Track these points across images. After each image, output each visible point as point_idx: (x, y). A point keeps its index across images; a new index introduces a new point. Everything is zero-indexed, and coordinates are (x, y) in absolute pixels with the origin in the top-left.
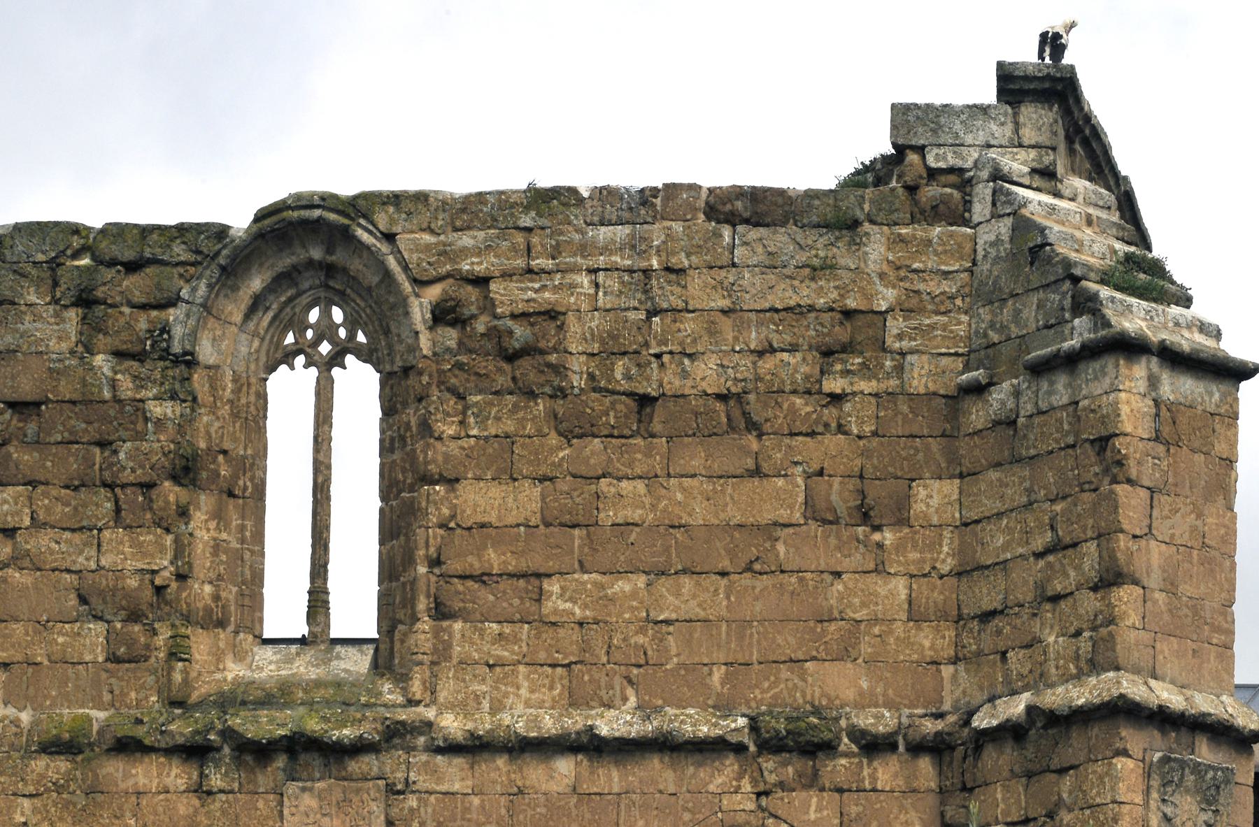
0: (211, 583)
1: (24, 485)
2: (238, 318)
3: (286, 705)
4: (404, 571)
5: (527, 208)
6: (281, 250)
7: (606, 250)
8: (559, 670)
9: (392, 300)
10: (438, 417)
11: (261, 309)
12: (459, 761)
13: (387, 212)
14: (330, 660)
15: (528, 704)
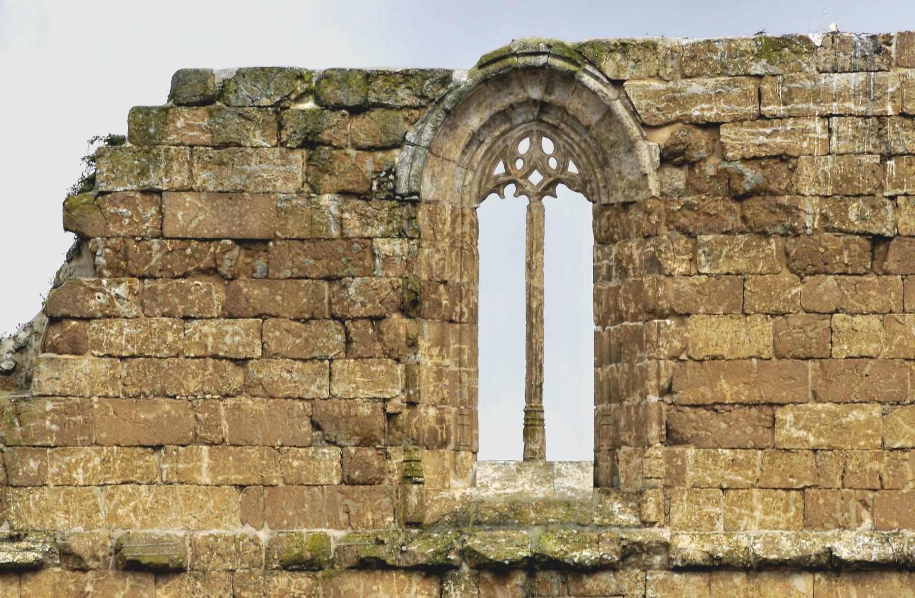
0: (434, 406)
1: (255, 317)
2: (456, 154)
3: (521, 525)
4: (628, 395)
5: (758, 56)
6: (499, 90)
7: (839, 96)
8: (793, 493)
9: (612, 138)
10: (669, 255)
11: (475, 142)
12: (696, 579)
13: (614, 59)
14: (553, 478)
15: (762, 525)
